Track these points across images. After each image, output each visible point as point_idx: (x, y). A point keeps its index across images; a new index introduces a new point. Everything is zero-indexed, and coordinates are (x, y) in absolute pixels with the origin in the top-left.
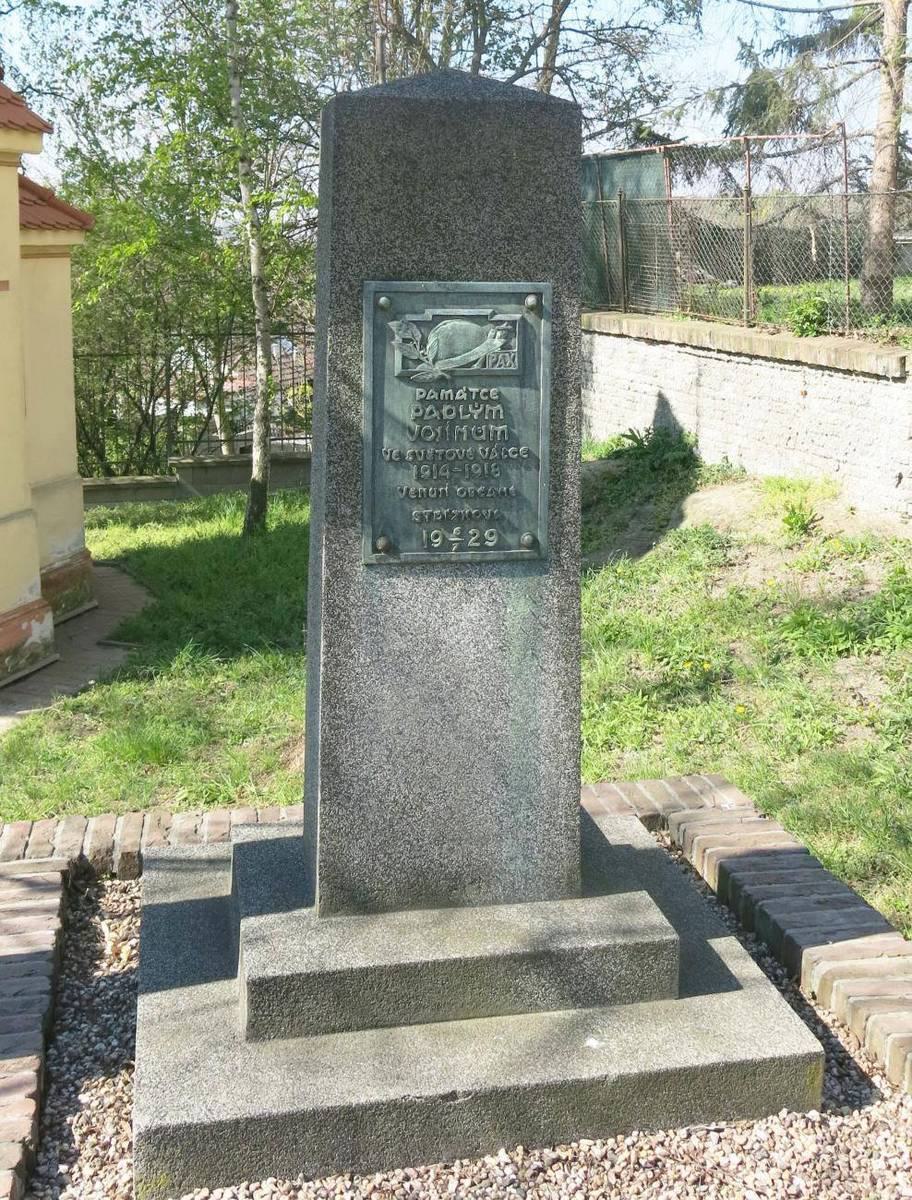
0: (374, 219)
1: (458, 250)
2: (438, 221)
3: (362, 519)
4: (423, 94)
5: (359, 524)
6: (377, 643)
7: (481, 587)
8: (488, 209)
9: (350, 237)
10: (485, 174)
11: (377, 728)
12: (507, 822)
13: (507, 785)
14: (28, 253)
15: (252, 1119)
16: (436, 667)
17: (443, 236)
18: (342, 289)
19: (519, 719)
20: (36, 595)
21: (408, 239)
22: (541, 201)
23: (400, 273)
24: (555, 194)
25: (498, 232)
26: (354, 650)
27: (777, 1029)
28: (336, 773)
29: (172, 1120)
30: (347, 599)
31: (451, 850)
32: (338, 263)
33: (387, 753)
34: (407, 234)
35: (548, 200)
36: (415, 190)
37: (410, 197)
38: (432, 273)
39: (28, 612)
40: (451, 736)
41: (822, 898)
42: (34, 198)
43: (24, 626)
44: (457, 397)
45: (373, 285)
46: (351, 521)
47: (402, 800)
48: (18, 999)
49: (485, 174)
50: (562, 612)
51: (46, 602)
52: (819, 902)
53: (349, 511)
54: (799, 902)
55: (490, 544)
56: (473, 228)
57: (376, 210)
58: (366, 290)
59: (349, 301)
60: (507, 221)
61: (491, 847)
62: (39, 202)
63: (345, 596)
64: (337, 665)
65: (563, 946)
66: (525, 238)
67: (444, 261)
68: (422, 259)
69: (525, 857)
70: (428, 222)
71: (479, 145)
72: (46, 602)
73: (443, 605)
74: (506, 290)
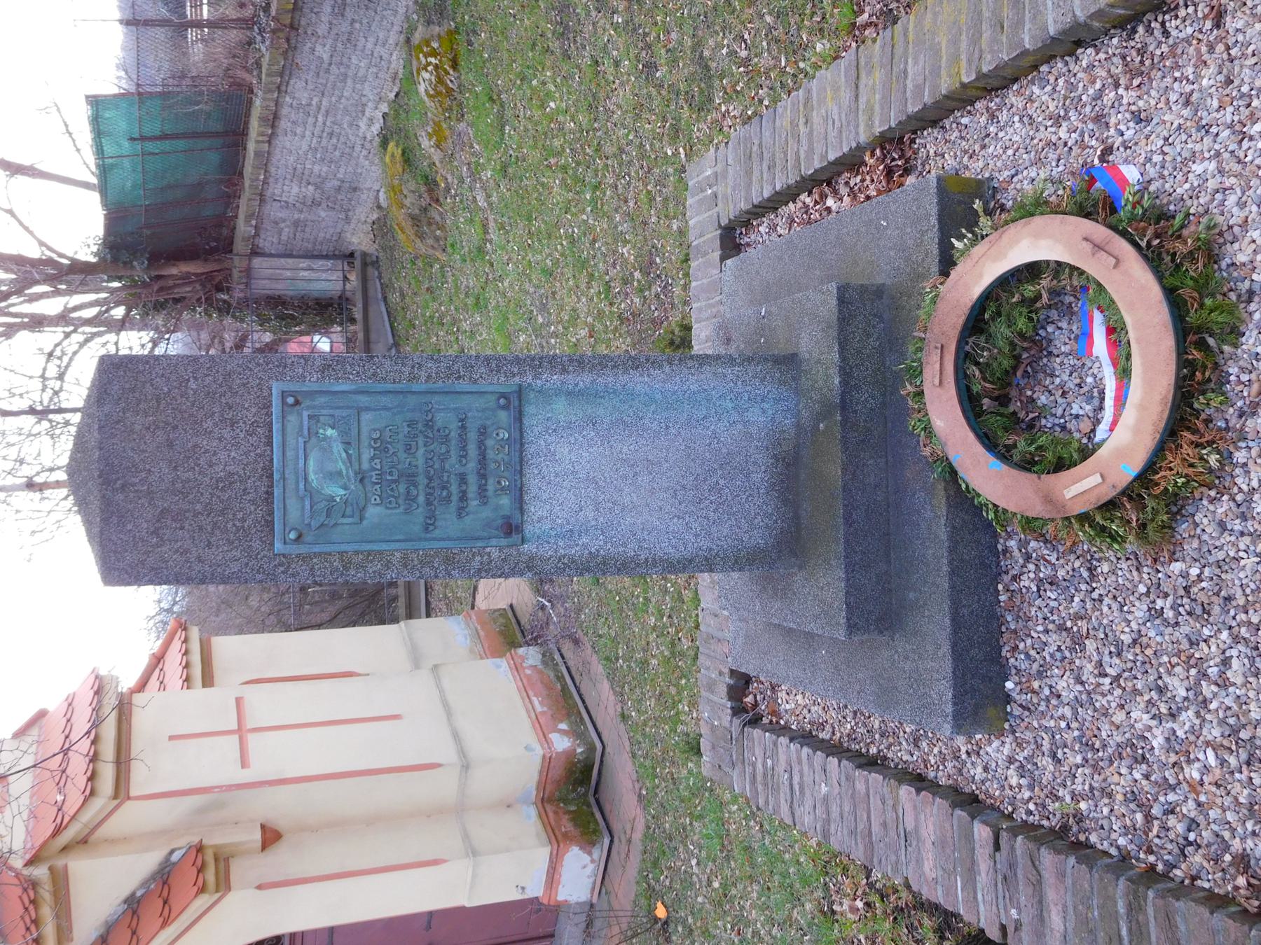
0: (218, 547)
1: (244, 469)
2: (217, 488)
3: (484, 548)
4: (96, 505)
5: (488, 550)
6: (587, 531)
7: (542, 442)
8: (205, 443)
9: (235, 567)
10: (170, 445)
11: (655, 528)
12: (735, 417)
13: (705, 417)
14: (208, 681)
15: (953, 648)
16: (608, 480)
17: (231, 483)
18: (283, 572)
19: (652, 408)
20: (503, 664)
21: (234, 515)
22: (195, 393)
23: (266, 521)
24: (188, 380)
25: (227, 433)
26: (593, 550)
27: (914, 209)
28: (690, 561)
29: (949, 709)
30: (551, 556)
31: (755, 463)
32: (259, 577)
33: (676, 520)
34: (231, 517)
35: (194, 387)
36: (188, 511)
37: (196, 514)
38: (267, 493)
39: (517, 668)
40: (665, 465)
41: (802, 120)
42: (157, 671)
43: (528, 672)
44: (379, 467)
45: (278, 546)
46: (486, 557)
47: (714, 506)
48: (843, 784)
49: (170, 445)
50: (564, 371)
51: (508, 654)
52: (806, 123)
53: (477, 558)
54: (804, 141)
55: (507, 436)
56: (223, 456)
57: (209, 545)
58: (283, 552)
59: (293, 566)
60: (216, 425)
61: (754, 430)
62: (160, 666)
63: (549, 559)
64: (604, 564)
65: (837, 382)
66: (230, 408)
67: (254, 482)
68: (253, 502)
69: (763, 401)
70: (219, 497)
71: (144, 451)
72: (508, 654)
73: (557, 475)
74: (280, 425)
